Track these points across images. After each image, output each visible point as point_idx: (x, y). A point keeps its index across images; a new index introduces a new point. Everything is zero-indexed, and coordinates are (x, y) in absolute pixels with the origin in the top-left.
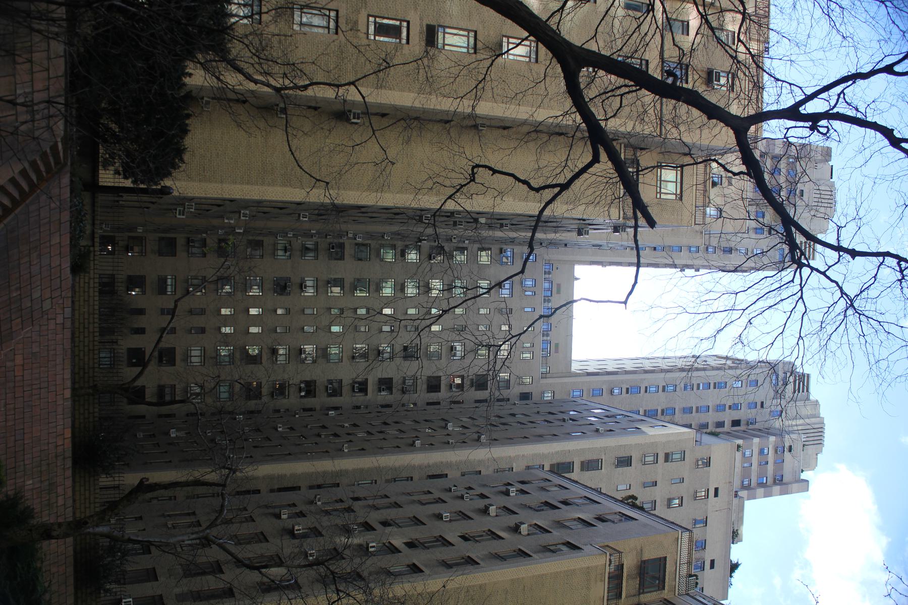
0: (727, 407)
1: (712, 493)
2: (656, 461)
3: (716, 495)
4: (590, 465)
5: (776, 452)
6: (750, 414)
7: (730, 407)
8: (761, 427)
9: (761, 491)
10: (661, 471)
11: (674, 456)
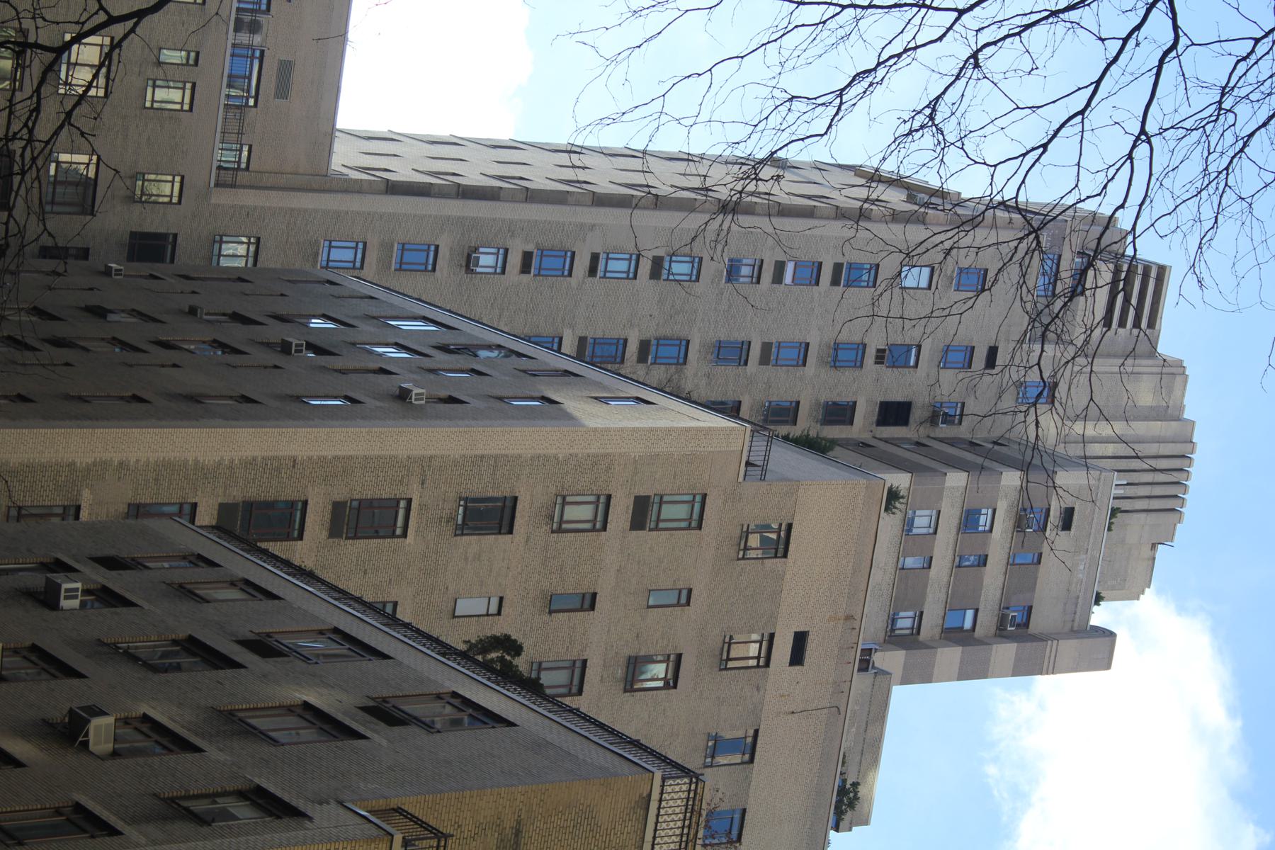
1: (783, 648)
2: (601, 524)
3: (797, 657)
4: (368, 518)
6: (950, 384)
9: (951, 655)
10: (617, 559)
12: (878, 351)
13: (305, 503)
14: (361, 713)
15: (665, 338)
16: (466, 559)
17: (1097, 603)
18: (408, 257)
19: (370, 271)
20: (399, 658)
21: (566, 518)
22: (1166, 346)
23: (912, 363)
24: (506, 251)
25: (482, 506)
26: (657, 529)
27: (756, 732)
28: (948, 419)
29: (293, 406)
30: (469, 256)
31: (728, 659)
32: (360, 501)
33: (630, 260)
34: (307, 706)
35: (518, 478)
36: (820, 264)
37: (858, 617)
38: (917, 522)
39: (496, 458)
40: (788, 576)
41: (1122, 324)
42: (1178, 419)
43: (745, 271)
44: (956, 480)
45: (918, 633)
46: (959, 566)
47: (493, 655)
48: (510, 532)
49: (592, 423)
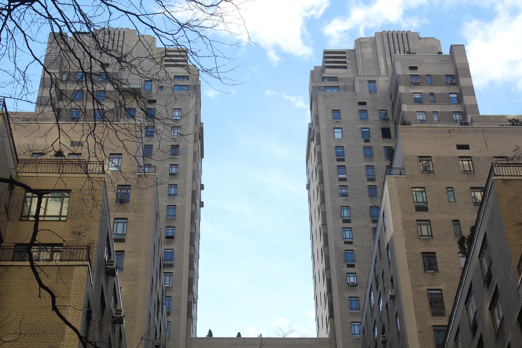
0: (366, 144)
1: (464, 153)
2: (428, 222)
3: (466, 147)
4: (436, 303)
5: (417, 84)
6: (374, 117)
7: (367, 141)
8: (390, 104)
9: (467, 100)
10: (439, 215)
11: (420, 199)
12: (365, 142)
13: (434, 326)
14: (490, 288)
15: (371, 215)
16: (447, 267)
17: (441, 53)
18: (354, 307)
19: (358, 319)
20: (471, 279)
21: (427, 234)
22: (351, 46)
23: (368, 130)
24: (348, 273)
25: (427, 264)
26: (426, 202)
27: (495, 157)
28: (386, 115)
29: (401, 335)
30: (351, 286)
31: (470, 171)
32: (430, 307)
33: (345, 231)
34: (490, 308)
35: (415, 253)
36: (338, 166)
37: (449, 129)
38: (421, 118)
39: (409, 261)
40: (438, 155)
41: (345, 62)
42: (375, 38)
43: (344, 191)
44: (405, 108)
45: (460, 112)
46: (435, 102)
47: (466, 246)
48: (435, 253)
49: (392, 230)
